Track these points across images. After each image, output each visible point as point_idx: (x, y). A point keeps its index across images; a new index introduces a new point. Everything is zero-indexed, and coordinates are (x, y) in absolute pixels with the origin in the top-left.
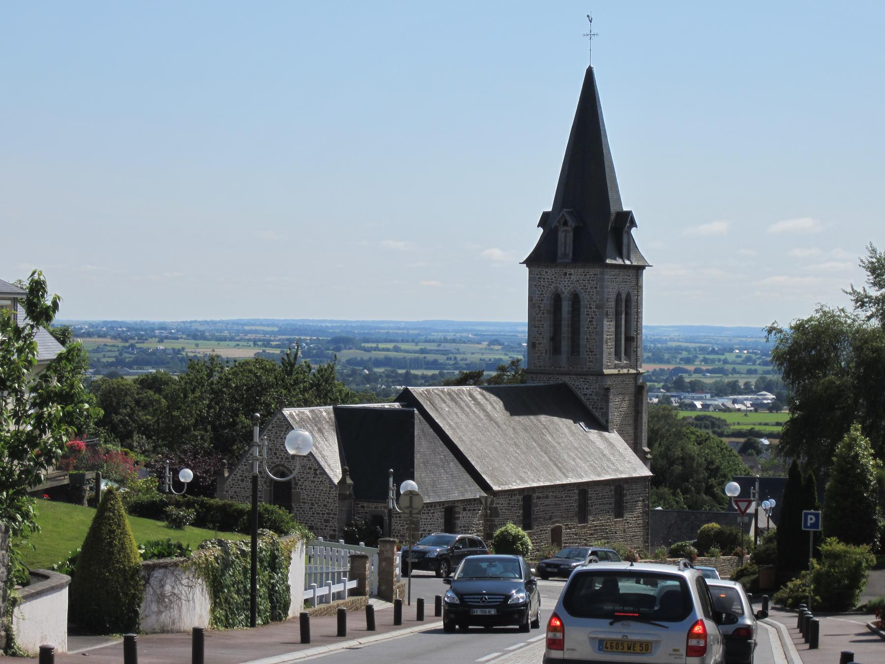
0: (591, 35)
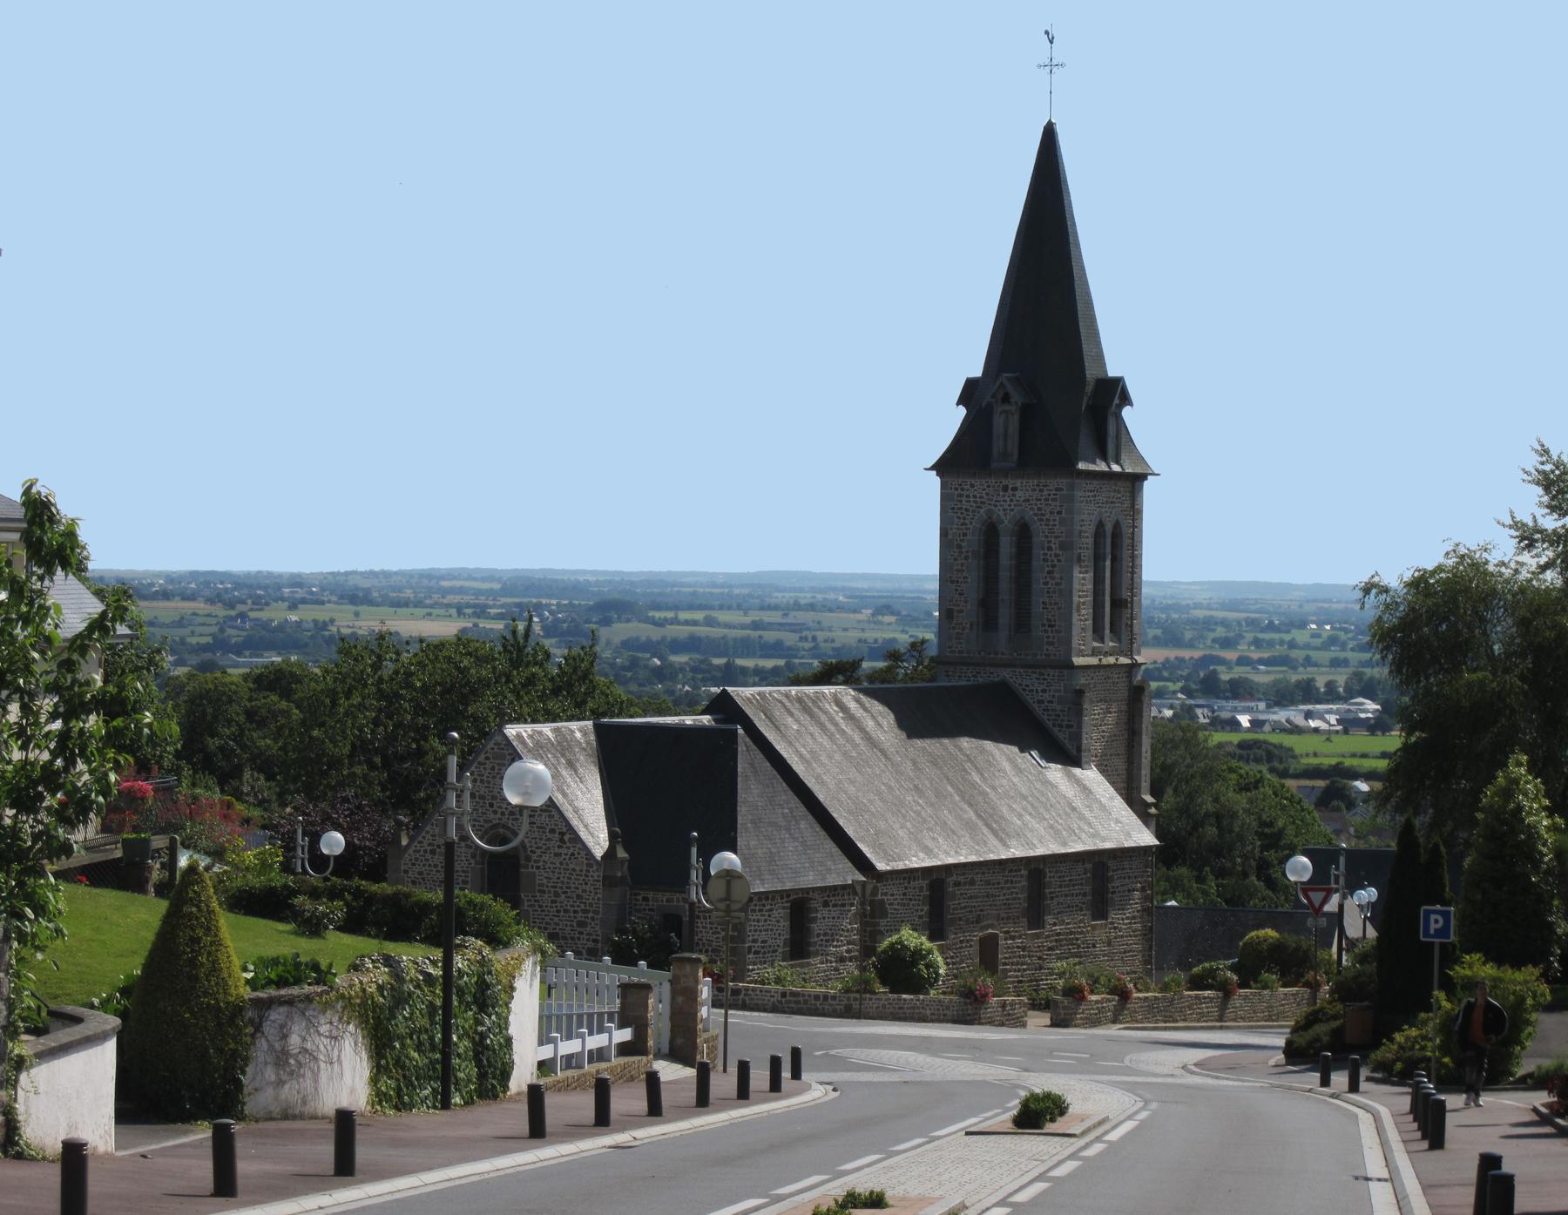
0: (1051, 66)
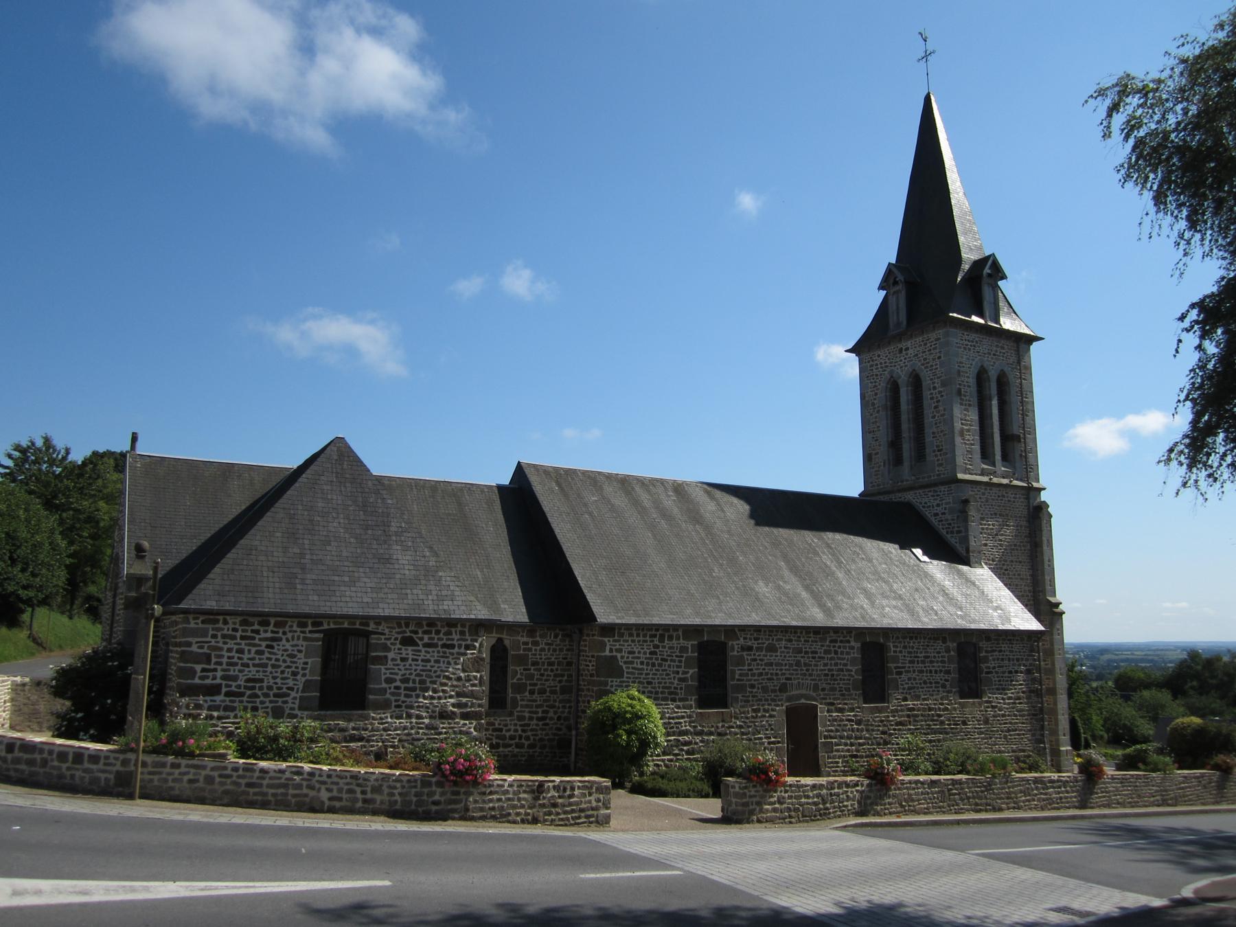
0: (926, 56)
